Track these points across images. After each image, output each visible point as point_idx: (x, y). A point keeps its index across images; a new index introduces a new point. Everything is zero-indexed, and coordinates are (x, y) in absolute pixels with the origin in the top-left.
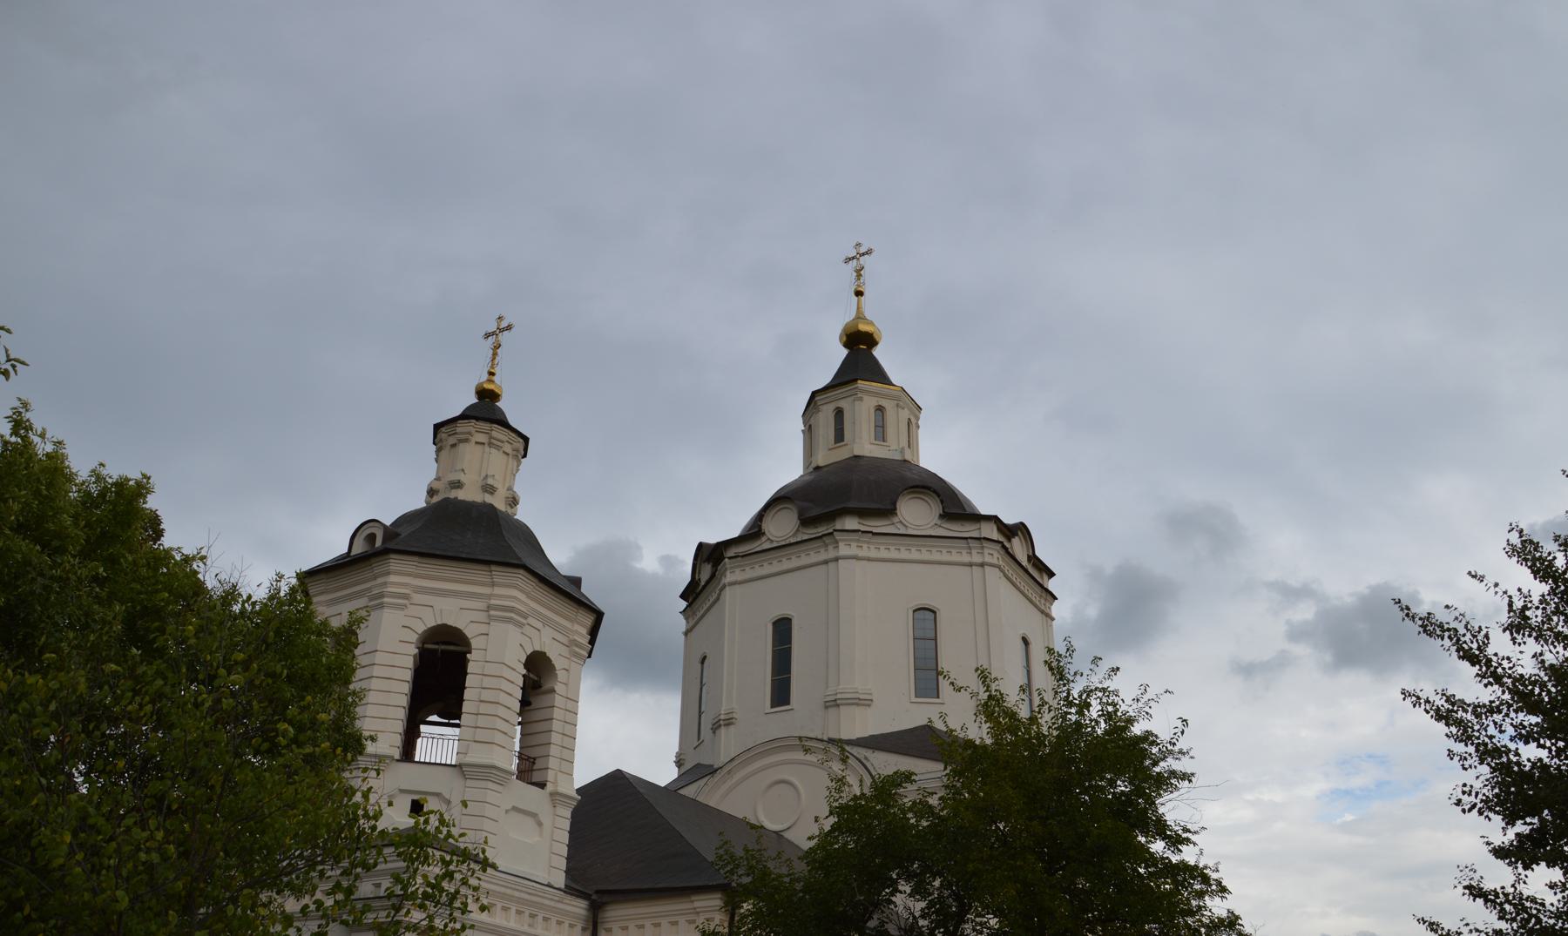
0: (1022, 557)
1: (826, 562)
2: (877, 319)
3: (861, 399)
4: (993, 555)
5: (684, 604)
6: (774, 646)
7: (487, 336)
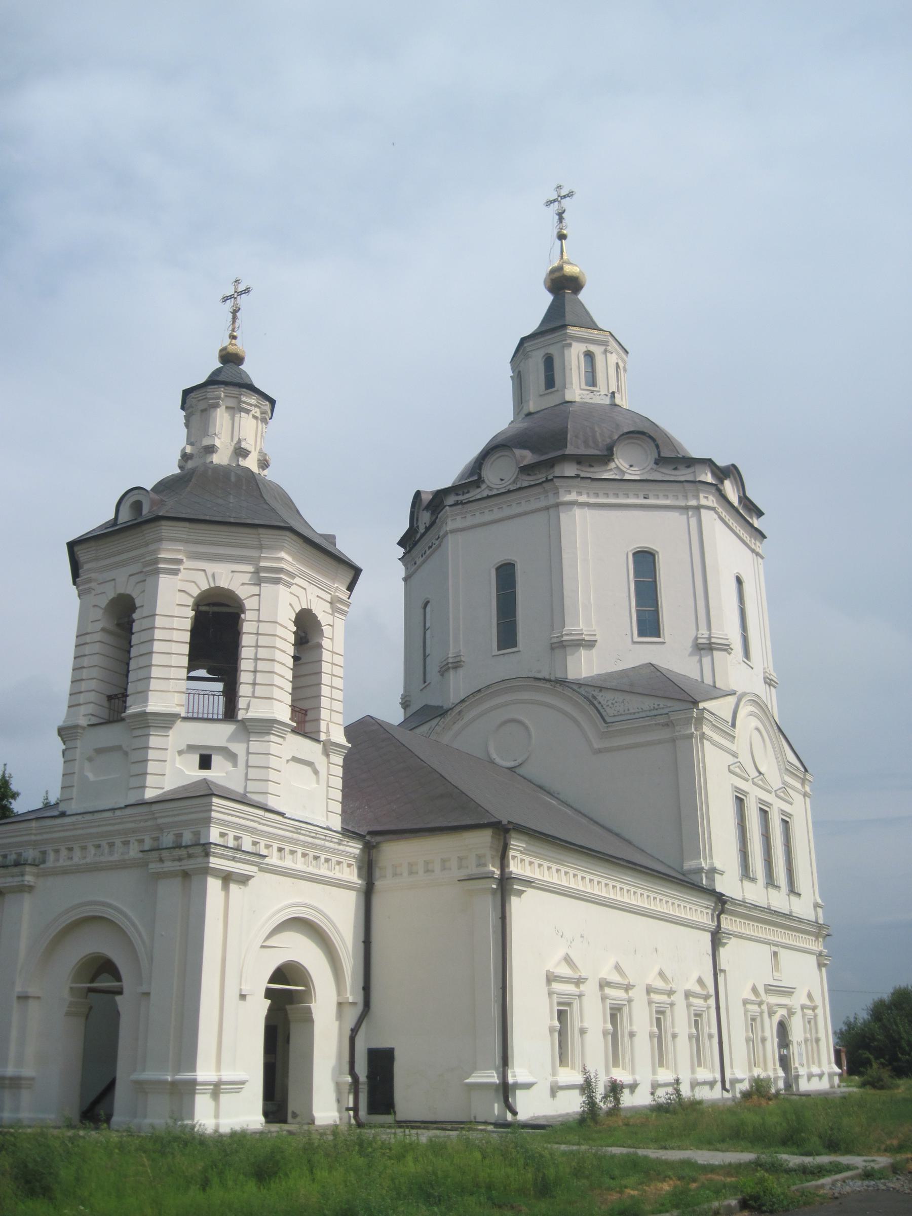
0: (734, 498)
1: (547, 508)
3: (570, 345)
4: (708, 499)
5: (401, 551)
6: (497, 591)
7: (225, 299)
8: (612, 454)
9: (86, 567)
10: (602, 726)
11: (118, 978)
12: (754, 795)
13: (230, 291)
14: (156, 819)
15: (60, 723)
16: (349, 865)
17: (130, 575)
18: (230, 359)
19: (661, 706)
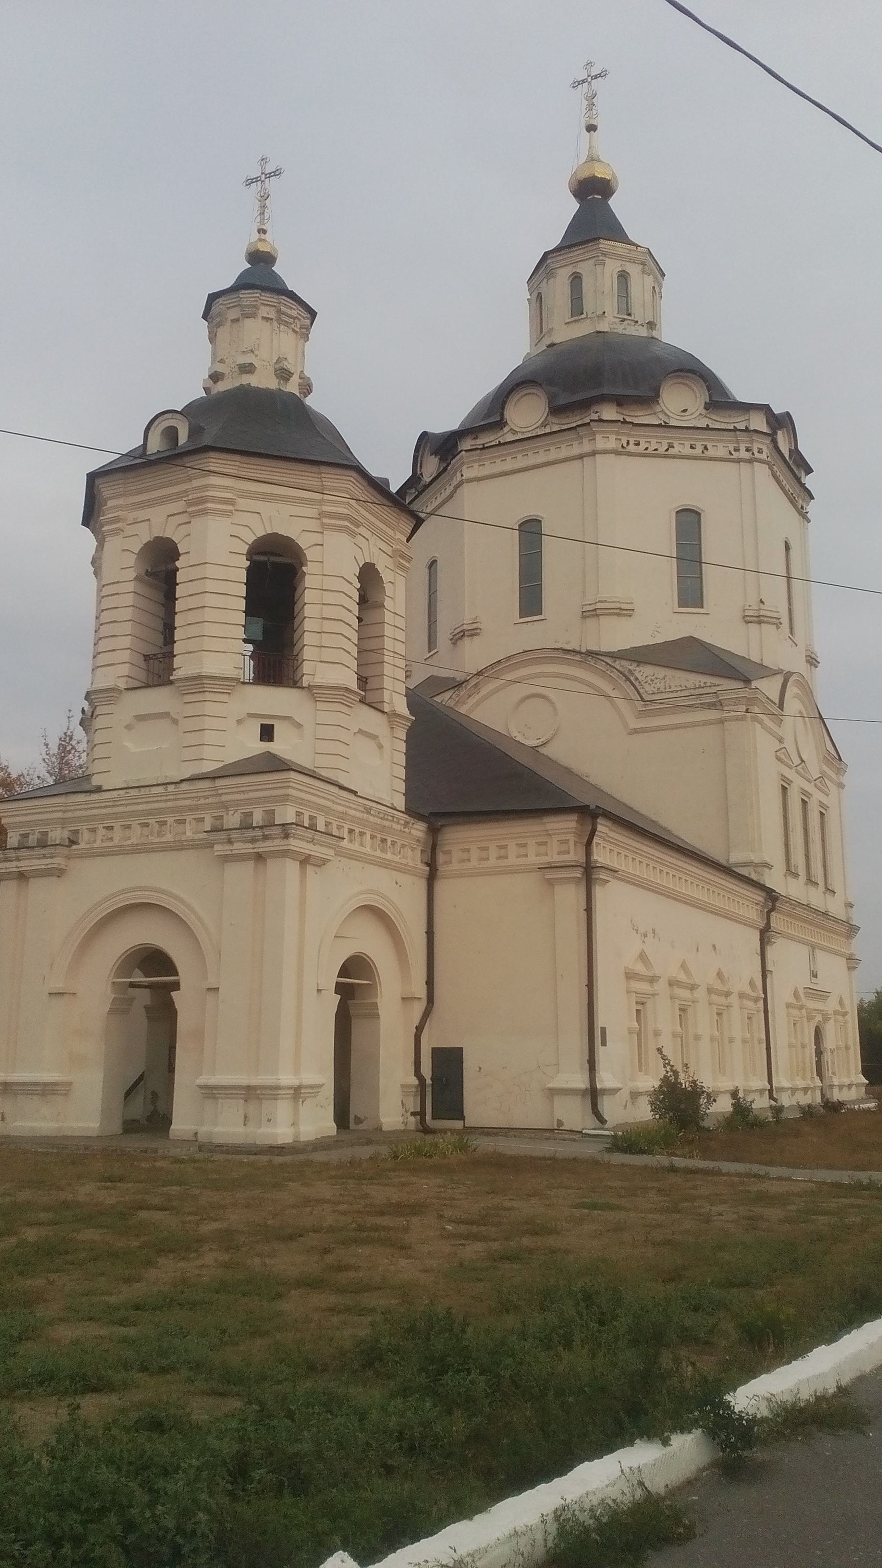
1: (581, 457)
2: (614, 164)
4: (762, 445)
8: (658, 395)
9: (110, 503)
10: (640, 705)
12: (798, 783)
14: (220, 795)
15: (86, 686)
16: (413, 849)
17: (168, 516)
18: (261, 260)
19: (708, 684)
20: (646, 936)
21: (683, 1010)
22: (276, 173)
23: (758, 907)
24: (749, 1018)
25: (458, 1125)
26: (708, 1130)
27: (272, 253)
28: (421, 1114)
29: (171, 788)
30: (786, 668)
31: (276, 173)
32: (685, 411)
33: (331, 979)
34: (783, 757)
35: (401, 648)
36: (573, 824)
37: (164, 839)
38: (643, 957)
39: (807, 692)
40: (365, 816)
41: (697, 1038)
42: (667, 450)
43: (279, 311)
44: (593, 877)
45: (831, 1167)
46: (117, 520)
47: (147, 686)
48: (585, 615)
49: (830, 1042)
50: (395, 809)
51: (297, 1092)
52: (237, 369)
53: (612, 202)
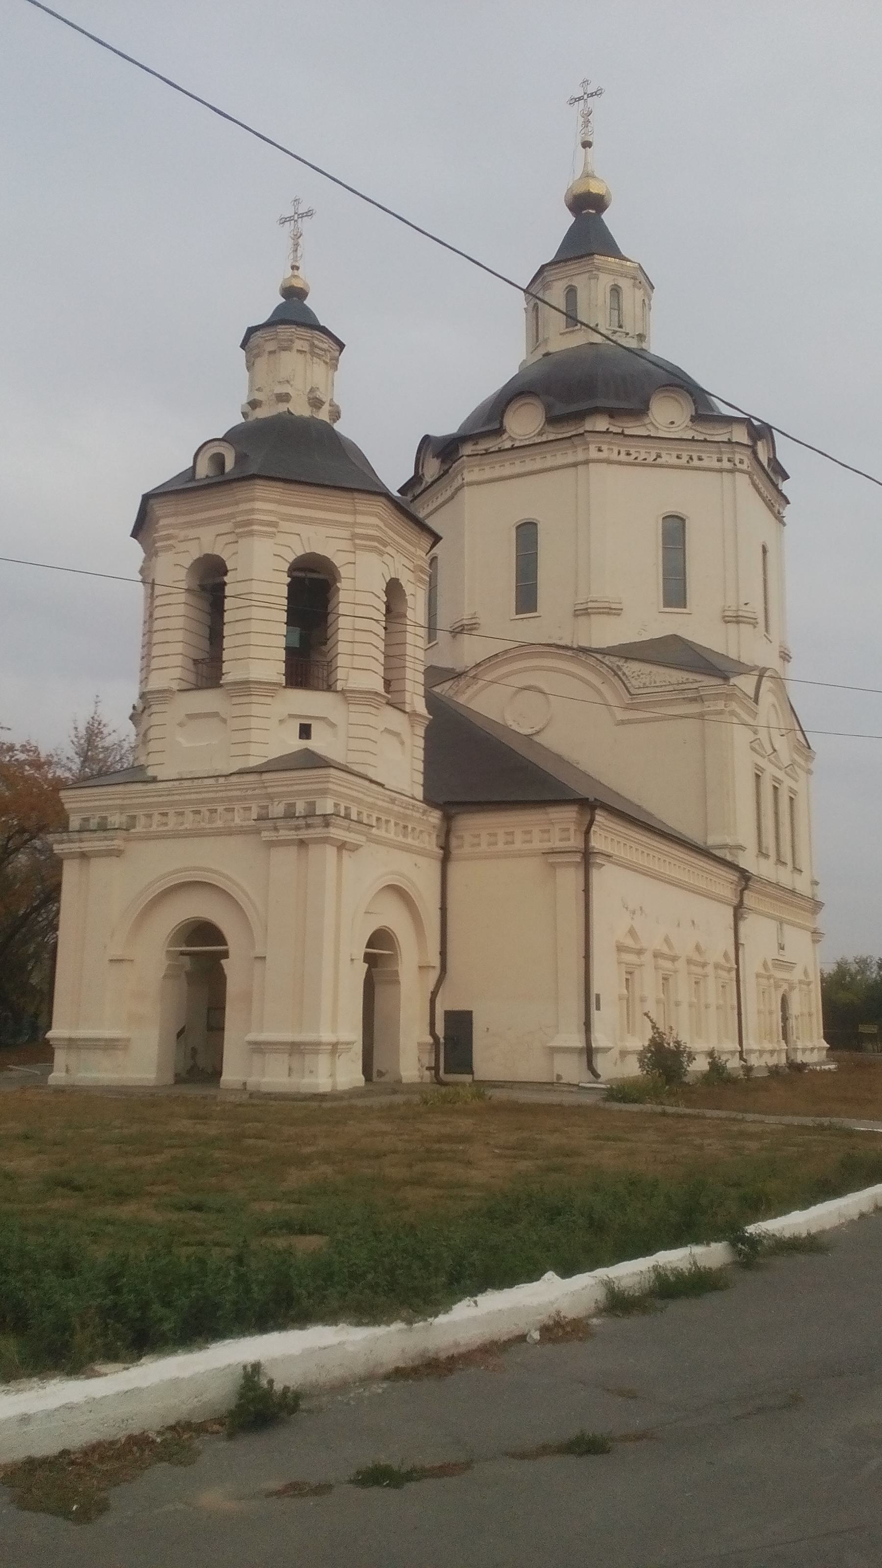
1: (575, 465)
4: (743, 457)
8: (648, 409)
9: (162, 522)
11: (222, 940)
12: (771, 770)
13: (289, 213)
14: (266, 787)
16: (430, 834)
17: (218, 535)
18: (294, 295)
19: (691, 680)
20: (634, 913)
21: (665, 979)
22: (309, 214)
23: (733, 886)
24: (696, 983)
25: (467, 1078)
26: (688, 1084)
27: (305, 288)
28: (436, 1068)
29: (222, 780)
30: (761, 664)
31: (309, 214)
32: (672, 423)
33: (360, 951)
34: (757, 747)
35: (420, 654)
36: (574, 815)
37: (214, 826)
38: (632, 932)
39: (779, 680)
40: (390, 806)
41: (677, 1004)
42: (655, 460)
43: (313, 345)
44: (591, 861)
45: (796, 1114)
46: (169, 537)
47: (198, 688)
48: (577, 614)
49: (795, 1009)
50: (414, 798)
51: (335, 1048)
52: (274, 397)
53: (606, 216)
